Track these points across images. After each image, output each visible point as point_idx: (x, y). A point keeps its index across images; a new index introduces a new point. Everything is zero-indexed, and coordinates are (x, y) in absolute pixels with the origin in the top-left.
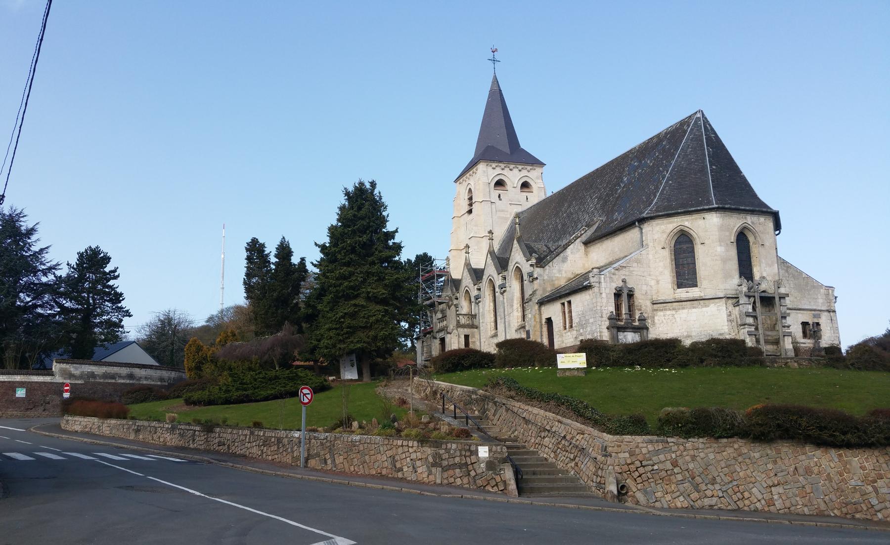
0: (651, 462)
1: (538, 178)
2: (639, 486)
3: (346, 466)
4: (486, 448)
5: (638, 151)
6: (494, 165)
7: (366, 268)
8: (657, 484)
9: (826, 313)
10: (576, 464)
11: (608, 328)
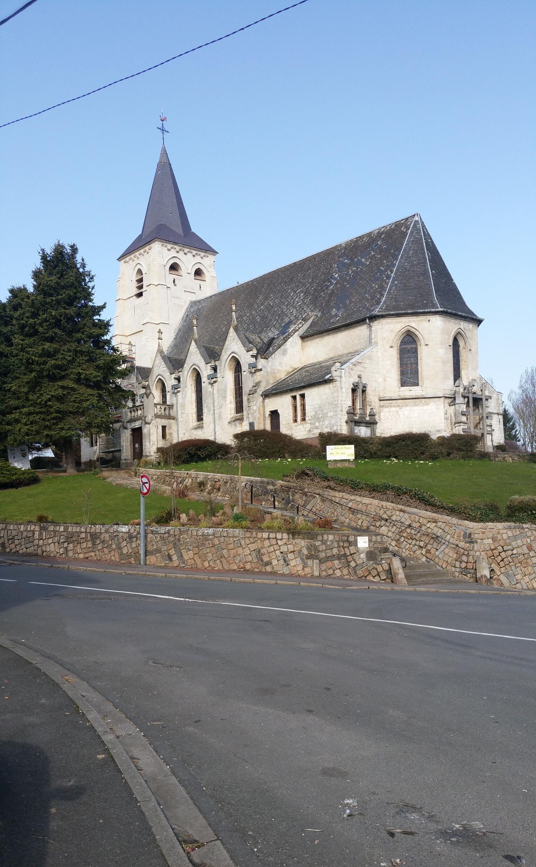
0: (510, 547)
1: (210, 266)
2: (503, 570)
3: (198, 561)
4: (366, 539)
5: (345, 248)
6: (169, 246)
7: (74, 345)
8: (516, 568)
9: (496, 416)
10: (428, 551)
11: (347, 422)
